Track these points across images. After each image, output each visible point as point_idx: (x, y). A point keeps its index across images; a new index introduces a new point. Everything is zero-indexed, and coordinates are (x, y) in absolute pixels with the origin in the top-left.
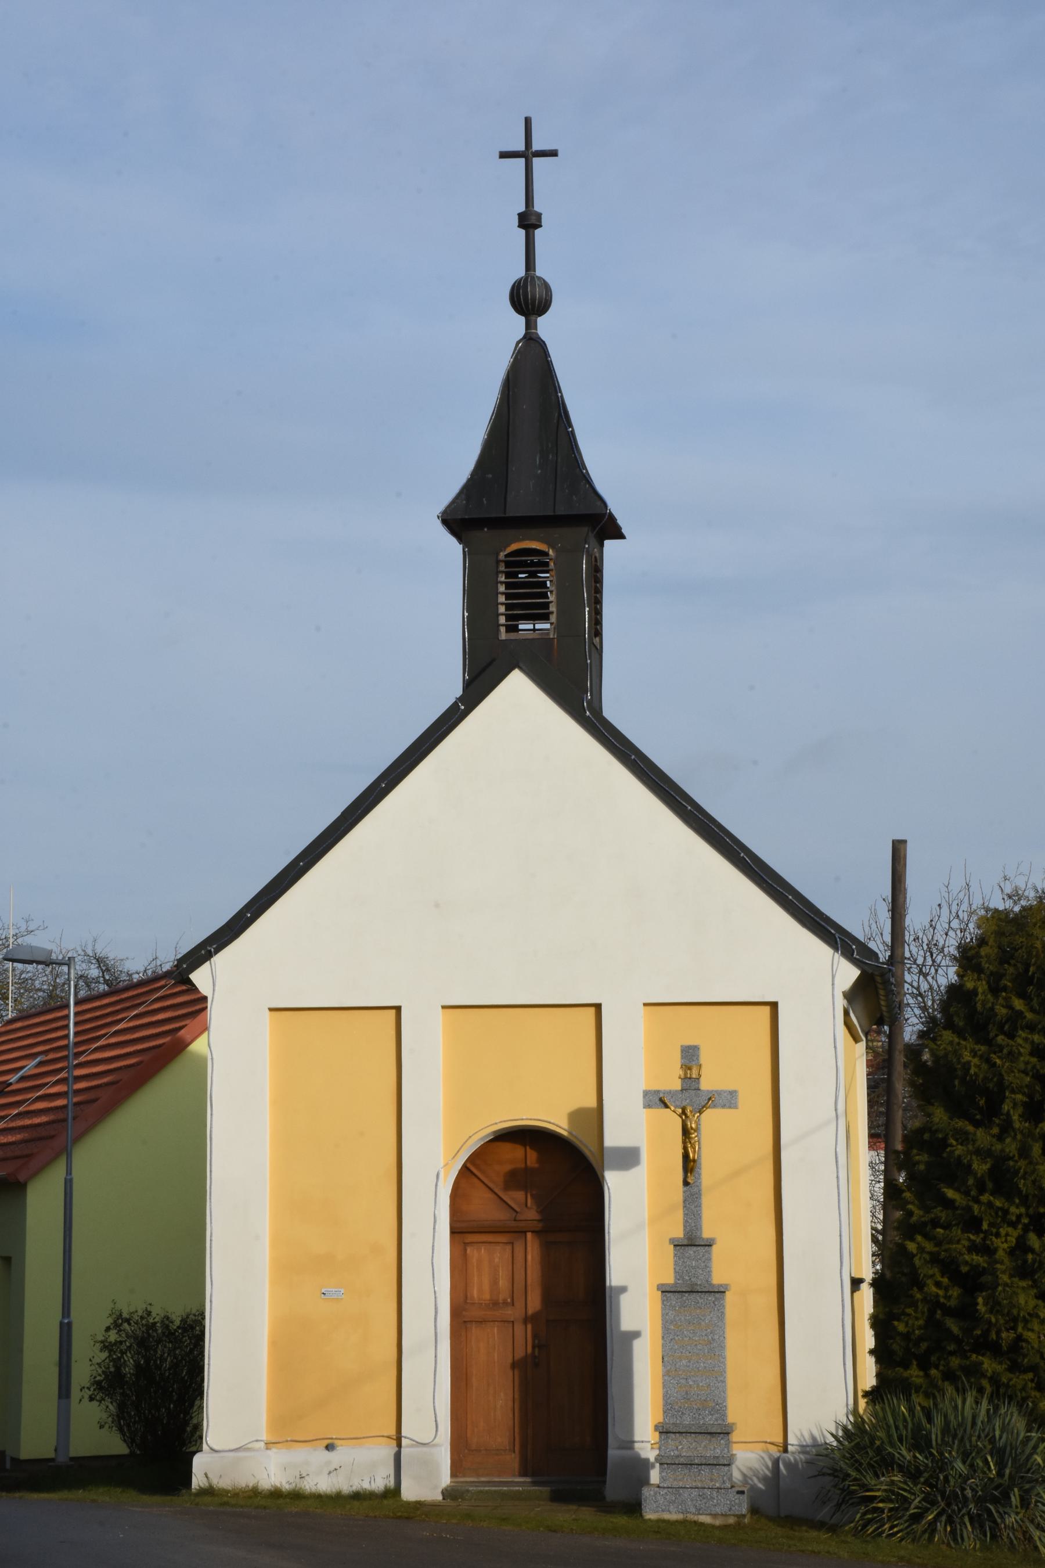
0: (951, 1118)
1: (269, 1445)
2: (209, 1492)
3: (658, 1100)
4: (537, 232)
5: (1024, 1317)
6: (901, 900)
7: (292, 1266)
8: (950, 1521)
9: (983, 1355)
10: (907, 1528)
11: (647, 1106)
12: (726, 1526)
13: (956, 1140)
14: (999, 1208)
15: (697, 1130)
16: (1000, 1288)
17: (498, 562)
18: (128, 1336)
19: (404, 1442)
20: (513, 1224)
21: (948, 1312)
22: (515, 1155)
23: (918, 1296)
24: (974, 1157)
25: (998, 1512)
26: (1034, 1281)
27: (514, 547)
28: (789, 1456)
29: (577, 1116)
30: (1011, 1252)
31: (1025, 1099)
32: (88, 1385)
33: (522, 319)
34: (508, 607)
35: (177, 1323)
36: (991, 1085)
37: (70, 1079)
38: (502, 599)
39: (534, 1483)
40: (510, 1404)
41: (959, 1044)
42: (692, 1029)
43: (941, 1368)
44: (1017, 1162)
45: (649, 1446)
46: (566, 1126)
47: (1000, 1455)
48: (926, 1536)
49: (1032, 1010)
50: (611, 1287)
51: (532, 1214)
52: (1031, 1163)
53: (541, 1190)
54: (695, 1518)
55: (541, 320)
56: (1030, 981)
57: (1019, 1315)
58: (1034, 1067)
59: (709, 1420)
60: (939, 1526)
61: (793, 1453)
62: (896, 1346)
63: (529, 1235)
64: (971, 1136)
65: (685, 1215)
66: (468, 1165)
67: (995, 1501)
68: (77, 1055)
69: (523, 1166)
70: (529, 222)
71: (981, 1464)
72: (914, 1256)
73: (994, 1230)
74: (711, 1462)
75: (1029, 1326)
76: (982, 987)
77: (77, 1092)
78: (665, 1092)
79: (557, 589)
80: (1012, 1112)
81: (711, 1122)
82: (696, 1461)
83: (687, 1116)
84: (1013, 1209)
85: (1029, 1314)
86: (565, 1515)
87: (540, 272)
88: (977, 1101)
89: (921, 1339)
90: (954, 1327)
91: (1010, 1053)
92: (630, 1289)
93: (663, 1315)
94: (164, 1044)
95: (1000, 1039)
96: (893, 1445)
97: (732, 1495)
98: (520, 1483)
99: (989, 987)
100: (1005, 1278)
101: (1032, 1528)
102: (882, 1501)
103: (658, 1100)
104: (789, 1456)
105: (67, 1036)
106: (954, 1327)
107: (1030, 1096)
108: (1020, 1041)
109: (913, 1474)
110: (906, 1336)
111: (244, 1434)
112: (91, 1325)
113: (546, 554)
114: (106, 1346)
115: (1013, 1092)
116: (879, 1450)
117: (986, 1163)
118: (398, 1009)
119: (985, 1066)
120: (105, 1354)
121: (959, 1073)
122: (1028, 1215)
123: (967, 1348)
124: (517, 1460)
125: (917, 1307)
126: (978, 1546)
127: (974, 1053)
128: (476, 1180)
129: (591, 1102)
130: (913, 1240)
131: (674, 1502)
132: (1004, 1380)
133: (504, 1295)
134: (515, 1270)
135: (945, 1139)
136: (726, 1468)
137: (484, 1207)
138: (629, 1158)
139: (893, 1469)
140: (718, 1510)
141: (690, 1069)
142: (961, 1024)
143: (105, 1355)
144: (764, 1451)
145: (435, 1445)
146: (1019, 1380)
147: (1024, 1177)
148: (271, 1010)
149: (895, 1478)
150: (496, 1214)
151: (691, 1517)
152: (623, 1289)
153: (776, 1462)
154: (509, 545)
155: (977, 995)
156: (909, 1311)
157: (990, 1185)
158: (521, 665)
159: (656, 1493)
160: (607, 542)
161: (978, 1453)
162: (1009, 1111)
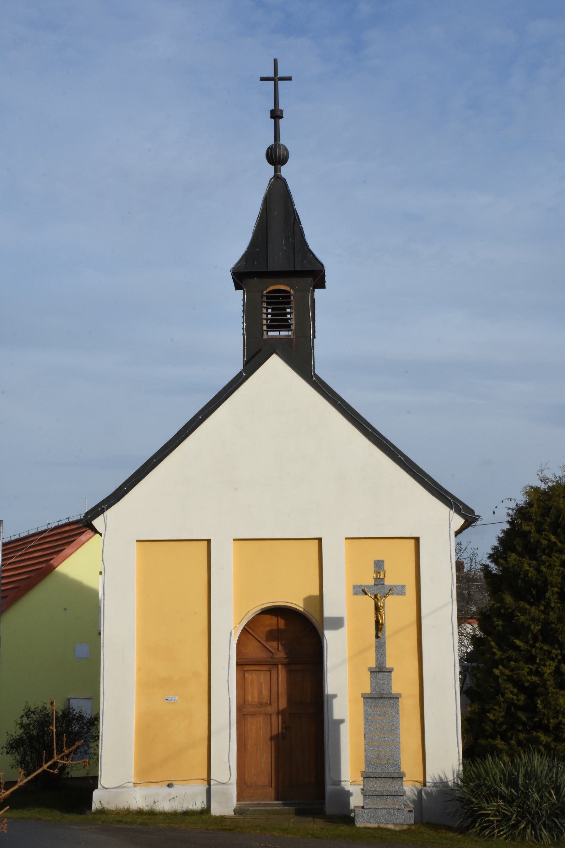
1: (135, 784)
2: (102, 812)
4: (281, 120)
7: (148, 684)
8: (534, 828)
10: (508, 832)
13: (520, 613)
14: (546, 650)
15: (383, 607)
16: (550, 695)
17: (262, 296)
19: (212, 782)
20: (271, 660)
22: (272, 622)
23: (502, 699)
27: (271, 288)
28: (427, 788)
29: (308, 600)
33: (273, 167)
36: (540, 583)
39: (284, 805)
40: (269, 760)
41: (519, 560)
42: (380, 551)
44: (556, 625)
45: (349, 783)
46: (302, 605)
49: (560, 541)
50: (328, 695)
51: (281, 655)
53: (288, 641)
54: (385, 826)
59: (391, 770)
61: (429, 787)
63: (280, 666)
64: (528, 611)
65: (377, 655)
69: (276, 628)
70: (276, 115)
71: (548, 795)
72: (498, 677)
74: (393, 794)
78: (365, 586)
79: (295, 311)
80: (551, 597)
81: (391, 604)
82: (385, 794)
83: (378, 600)
84: (554, 651)
87: (282, 141)
88: (533, 591)
92: (338, 696)
93: (364, 711)
104: (427, 788)
109: (510, 801)
110: (494, 722)
111: (122, 779)
113: (289, 292)
114: (22, 726)
115: (552, 586)
118: (209, 541)
120: (22, 730)
121: (522, 576)
122: (561, 654)
124: (274, 791)
128: (250, 636)
129: (316, 593)
130: (497, 668)
133: (266, 699)
134: (273, 685)
136: (401, 798)
137: (255, 651)
138: (337, 623)
139: (497, 798)
140: (398, 821)
141: (379, 573)
142: (520, 549)
144: (412, 786)
150: (260, 654)
152: (335, 696)
153: (420, 792)
154: (269, 287)
156: (496, 707)
157: (540, 638)
158: (277, 351)
159: (362, 812)
160: (316, 290)
162: (549, 597)
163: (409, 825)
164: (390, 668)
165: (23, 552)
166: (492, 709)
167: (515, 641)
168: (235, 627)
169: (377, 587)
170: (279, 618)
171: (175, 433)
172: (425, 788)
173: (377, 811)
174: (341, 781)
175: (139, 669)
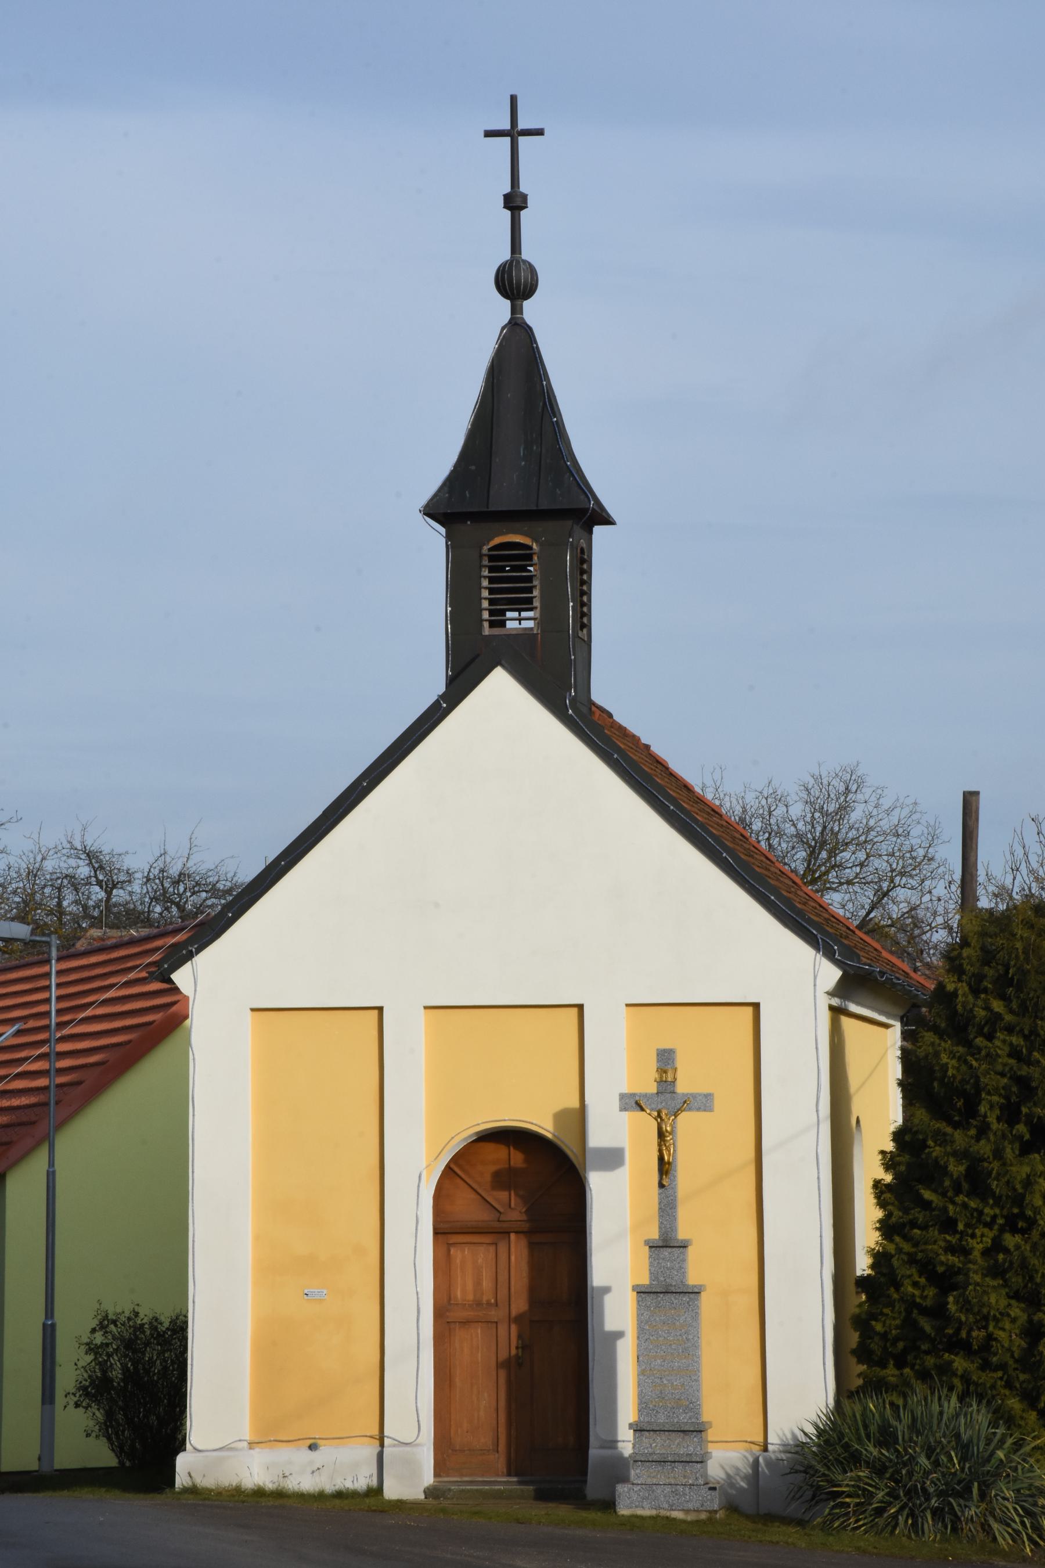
0: (930, 1120)
1: (252, 1445)
2: (193, 1490)
3: (634, 1103)
5: (995, 1316)
6: (972, 859)
7: (274, 1267)
8: (912, 1514)
9: (956, 1355)
11: (624, 1108)
12: (697, 1521)
13: (935, 1142)
16: (971, 1287)
17: (481, 556)
18: (114, 1338)
19: (387, 1441)
20: (497, 1224)
21: (924, 1311)
22: (498, 1155)
23: (896, 1296)
24: (952, 1160)
25: (960, 1505)
26: (1005, 1281)
27: (497, 541)
29: (561, 1117)
30: (986, 1253)
31: (1002, 1101)
32: (73, 1391)
33: (508, 303)
34: (492, 602)
35: (166, 1324)
36: (968, 1087)
37: (52, 1072)
38: (485, 593)
39: (519, 1483)
42: (670, 1032)
43: (917, 1367)
44: (990, 1163)
47: (965, 1450)
48: (890, 1528)
49: (1011, 1011)
51: (516, 1213)
52: (1004, 1164)
53: (523, 1191)
54: (668, 1514)
55: (526, 304)
56: (1010, 983)
57: (989, 1313)
58: (1011, 1069)
60: (901, 1519)
61: (774, 1452)
62: (875, 1346)
63: (513, 1236)
66: (452, 1166)
67: (958, 1495)
68: (61, 1025)
70: (515, 203)
71: (945, 1460)
72: (892, 1256)
73: (970, 1231)
75: (1000, 1325)
76: (963, 988)
77: (61, 1071)
78: (641, 1095)
79: (541, 583)
81: (687, 1125)
85: (1001, 1314)
86: (540, 1511)
87: (526, 254)
89: (896, 1339)
90: (926, 1325)
91: (988, 1055)
92: (614, 1289)
94: (154, 1021)
95: (979, 1041)
96: (859, 1440)
97: (704, 1491)
98: (503, 1482)
99: (970, 987)
100: (977, 1278)
101: (991, 1521)
102: (849, 1496)
103: (634, 1103)
105: (48, 1014)
106: (926, 1325)
107: (1007, 1098)
108: (997, 1043)
109: (879, 1469)
110: (884, 1336)
112: (75, 1326)
113: (530, 548)
114: (92, 1348)
115: (989, 1093)
116: (847, 1447)
117: (962, 1164)
119: (964, 1068)
120: (91, 1357)
121: (938, 1075)
123: (940, 1347)
125: (894, 1307)
126: (938, 1537)
127: (952, 1055)
128: (459, 1181)
129: (575, 1104)
131: (647, 1498)
132: (975, 1378)
133: (488, 1296)
134: (504, 1270)
135: (925, 1141)
136: (699, 1465)
137: (467, 1208)
138: (612, 1158)
140: (690, 1506)
141: (665, 1072)
143: (90, 1358)
145: (417, 1445)
146: (986, 1378)
147: (997, 1179)
148: (252, 1010)
149: (861, 1474)
151: (663, 1513)
152: (607, 1290)
153: (756, 1462)
154: (492, 539)
155: (957, 996)
156: (886, 1311)
157: (965, 1186)
158: (503, 662)
161: (943, 1448)
162: (986, 1113)
163: (710, 1512)
164: (682, 1241)
165: (132, 976)
166: (882, 1314)
167: (922, 1191)
168: (427, 1166)
169: (662, 1097)
170: (512, 1149)
171: (320, 813)
172: (766, 1454)
173: (654, 1487)
174: (617, 1441)
175: (257, 1238)
